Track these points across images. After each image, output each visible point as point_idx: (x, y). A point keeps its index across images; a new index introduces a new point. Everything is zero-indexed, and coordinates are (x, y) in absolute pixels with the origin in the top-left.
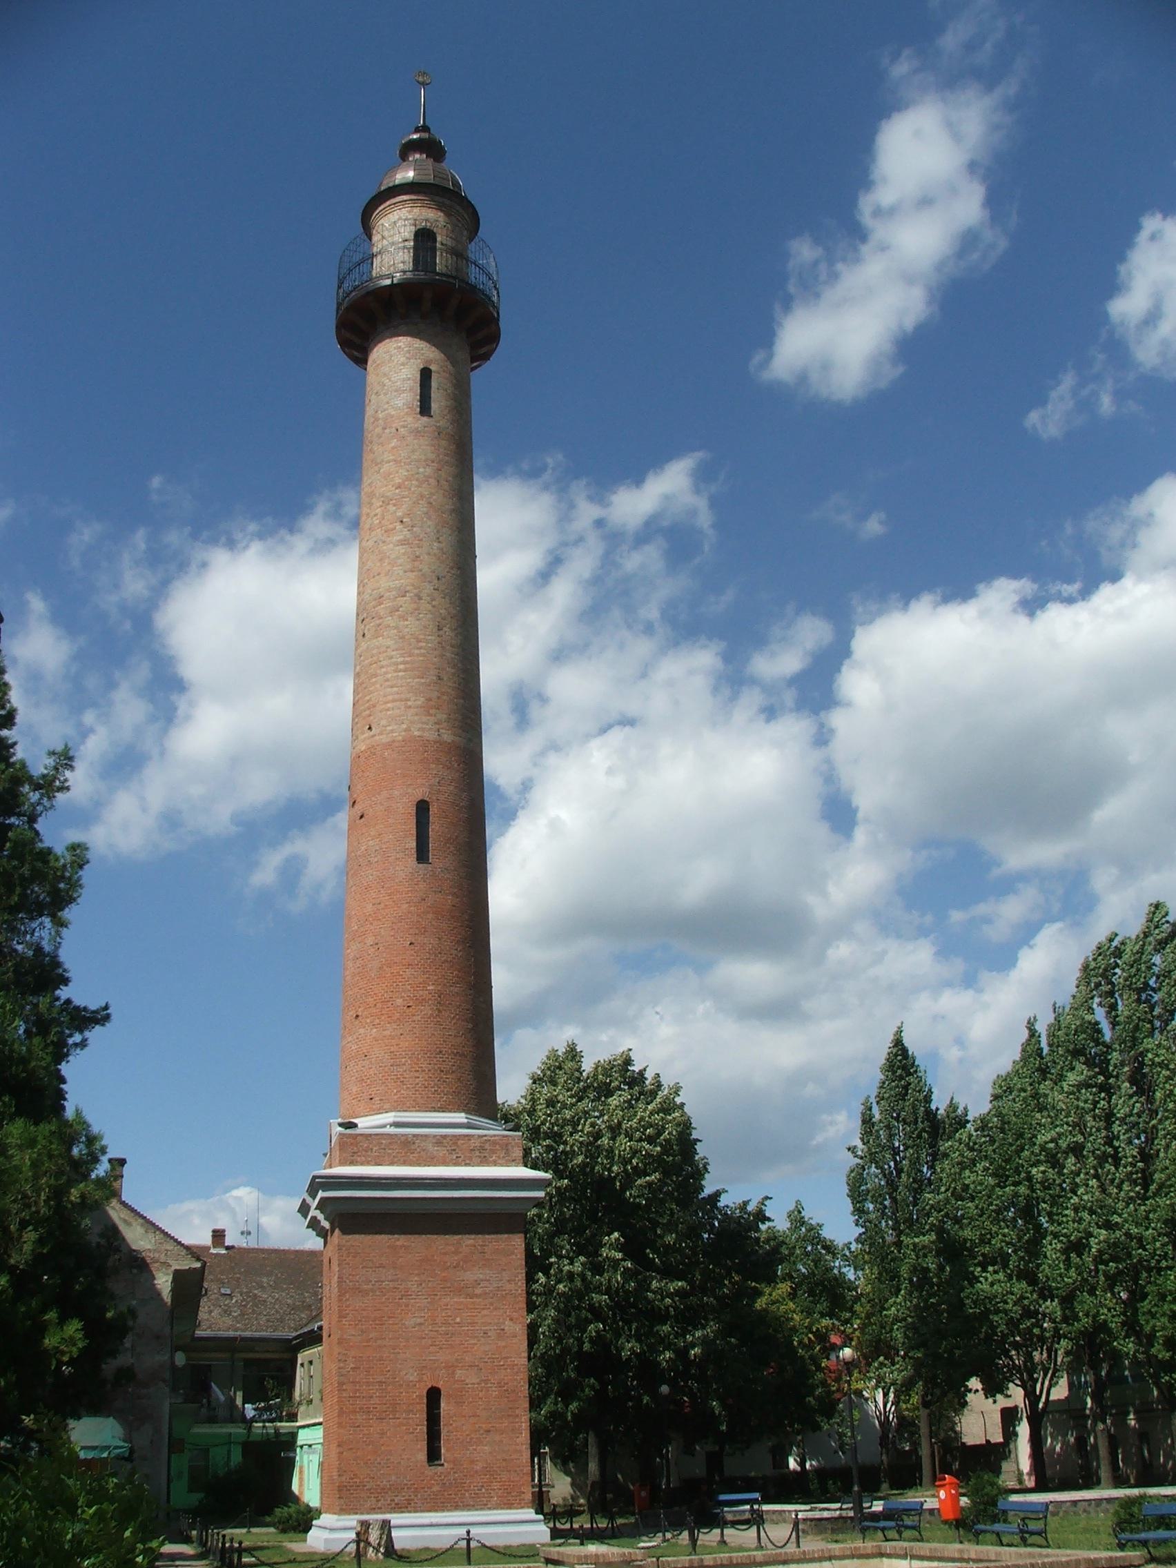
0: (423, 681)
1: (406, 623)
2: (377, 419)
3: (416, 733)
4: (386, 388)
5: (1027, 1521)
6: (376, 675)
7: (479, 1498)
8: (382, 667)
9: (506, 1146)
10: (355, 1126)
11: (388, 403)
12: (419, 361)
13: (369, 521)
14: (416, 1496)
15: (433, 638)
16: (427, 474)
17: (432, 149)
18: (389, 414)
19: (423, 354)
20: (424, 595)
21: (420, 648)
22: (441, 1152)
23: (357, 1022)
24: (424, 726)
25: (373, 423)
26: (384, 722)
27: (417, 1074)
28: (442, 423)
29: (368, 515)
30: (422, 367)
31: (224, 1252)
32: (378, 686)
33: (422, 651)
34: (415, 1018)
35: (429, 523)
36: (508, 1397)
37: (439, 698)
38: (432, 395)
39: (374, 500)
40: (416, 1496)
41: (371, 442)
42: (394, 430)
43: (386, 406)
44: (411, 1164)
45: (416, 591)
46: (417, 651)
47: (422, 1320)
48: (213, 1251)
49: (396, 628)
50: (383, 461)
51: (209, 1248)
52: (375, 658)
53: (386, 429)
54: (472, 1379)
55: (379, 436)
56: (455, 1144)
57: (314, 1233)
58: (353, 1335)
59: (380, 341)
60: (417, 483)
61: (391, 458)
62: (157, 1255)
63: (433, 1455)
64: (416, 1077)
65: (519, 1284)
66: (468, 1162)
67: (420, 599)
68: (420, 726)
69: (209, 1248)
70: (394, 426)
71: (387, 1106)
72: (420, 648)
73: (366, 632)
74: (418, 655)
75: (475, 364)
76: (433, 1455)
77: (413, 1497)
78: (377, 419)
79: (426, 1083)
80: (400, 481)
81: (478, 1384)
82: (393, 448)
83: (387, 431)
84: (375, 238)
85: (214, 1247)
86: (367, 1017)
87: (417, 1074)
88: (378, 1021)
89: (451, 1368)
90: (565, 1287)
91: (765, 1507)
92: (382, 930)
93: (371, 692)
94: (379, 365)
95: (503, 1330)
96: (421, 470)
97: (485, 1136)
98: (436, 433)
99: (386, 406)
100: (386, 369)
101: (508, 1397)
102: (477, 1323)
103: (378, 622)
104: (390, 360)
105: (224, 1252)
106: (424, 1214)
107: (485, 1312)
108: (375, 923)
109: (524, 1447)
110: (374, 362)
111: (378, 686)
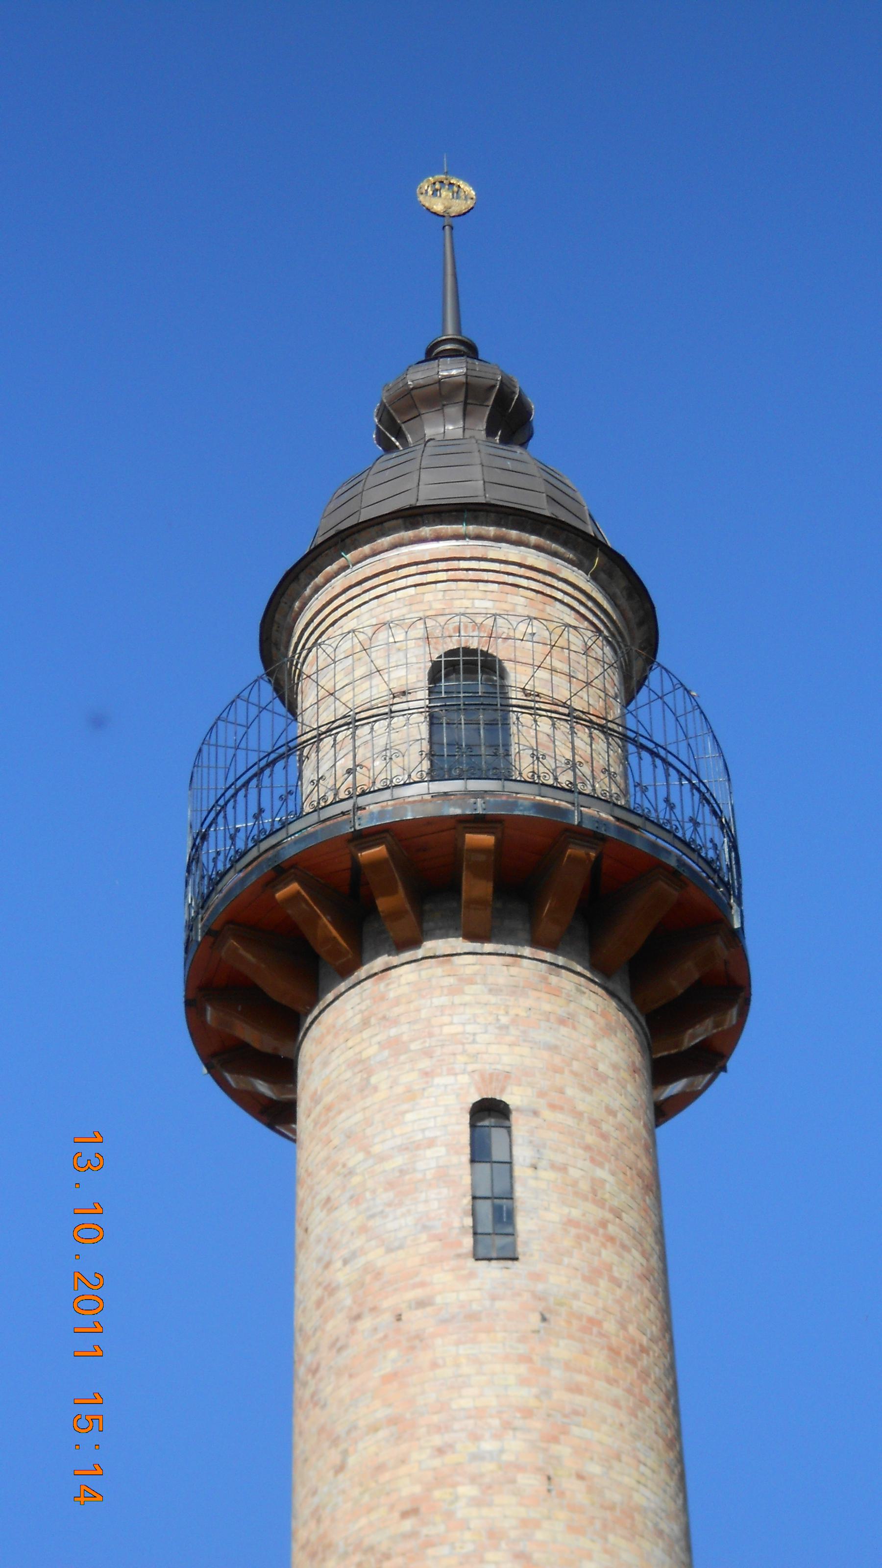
2: (331, 1290)
4: (356, 1180)
5: (289, 812)
11: (363, 1229)
12: (464, 1079)
13: (614, 799)
16: (505, 1457)
17: (469, 350)
18: (367, 1269)
19: (475, 1057)
25: (319, 1303)
30: (477, 1098)
38: (374, 825)
42: (387, 1318)
50: (354, 1427)
53: (358, 1317)
55: (338, 1347)
61: (381, 1413)
64: (473, 774)
70: (386, 1304)
78: (331, 1290)
80: (417, 1489)
82: (387, 1379)
83: (366, 1324)
94: (328, 1109)
98: (535, 1318)
99: (358, 1243)
100: (348, 1119)
104: (366, 1088)
106: (444, 246)
110: (316, 1099)
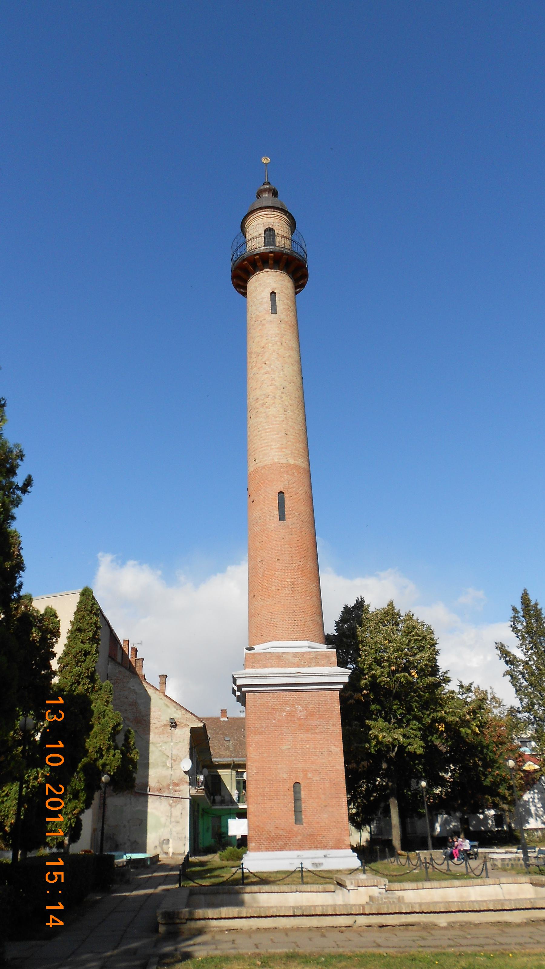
0: (278, 436)
1: (269, 410)
3: (277, 460)
6: (257, 435)
7: (322, 843)
8: (259, 431)
9: (327, 657)
10: (253, 649)
14: (290, 842)
15: (282, 416)
20: (277, 396)
21: (276, 421)
22: (296, 660)
23: (254, 599)
24: (280, 457)
26: (261, 457)
27: (283, 623)
28: (283, 316)
29: (250, 362)
31: (226, 719)
32: (258, 440)
33: (278, 422)
34: (281, 595)
35: (278, 363)
36: (335, 788)
37: (286, 443)
39: (252, 355)
40: (290, 842)
41: (250, 329)
42: (259, 322)
43: (255, 311)
44: (282, 667)
45: (273, 395)
46: (275, 423)
47: (289, 747)
48: (222, 719)
49: (265, 412)
51: (220, 718)
52: (256, 427)
54: (316, 778)
55: (253, 326)
56: (303, 656)
57: (241, 704)
58: (255, 755)
59: (399, 820)
60: (271, 345)
62: (182, 721)
63: (298, 820)
65: (338, 727)
66: (310, 665)
67: (275, 398)
68: (278, 457)
69: (219, 718)
71: (269, 639)
72: (276, 421)
73: (251, 416)
74: (275, 424)
75: (298, 290)
76: (298, 820)
77: (288, 843)
78: (252, 318)
79: (288, 627)
81: (319, 780)
83: (257, 322)
84: (247, 235)
85: (222, 717)
86: (259, 596)
87: (283, 623)
88: (263, 597)
89: (305, 772)
90: (486, 818)
91: (480, 850)
92: (264, 554)
93: (254, 444)
95: (331, 751)
96: (273, 339)
97: (318, 652)
101: (335, 788)
102: (317, 748)
103: (257, 411)
105: (226, 719)
107: (321, 742)
108: (261, 551)
109: (345, 815)
111: (258, 440)
